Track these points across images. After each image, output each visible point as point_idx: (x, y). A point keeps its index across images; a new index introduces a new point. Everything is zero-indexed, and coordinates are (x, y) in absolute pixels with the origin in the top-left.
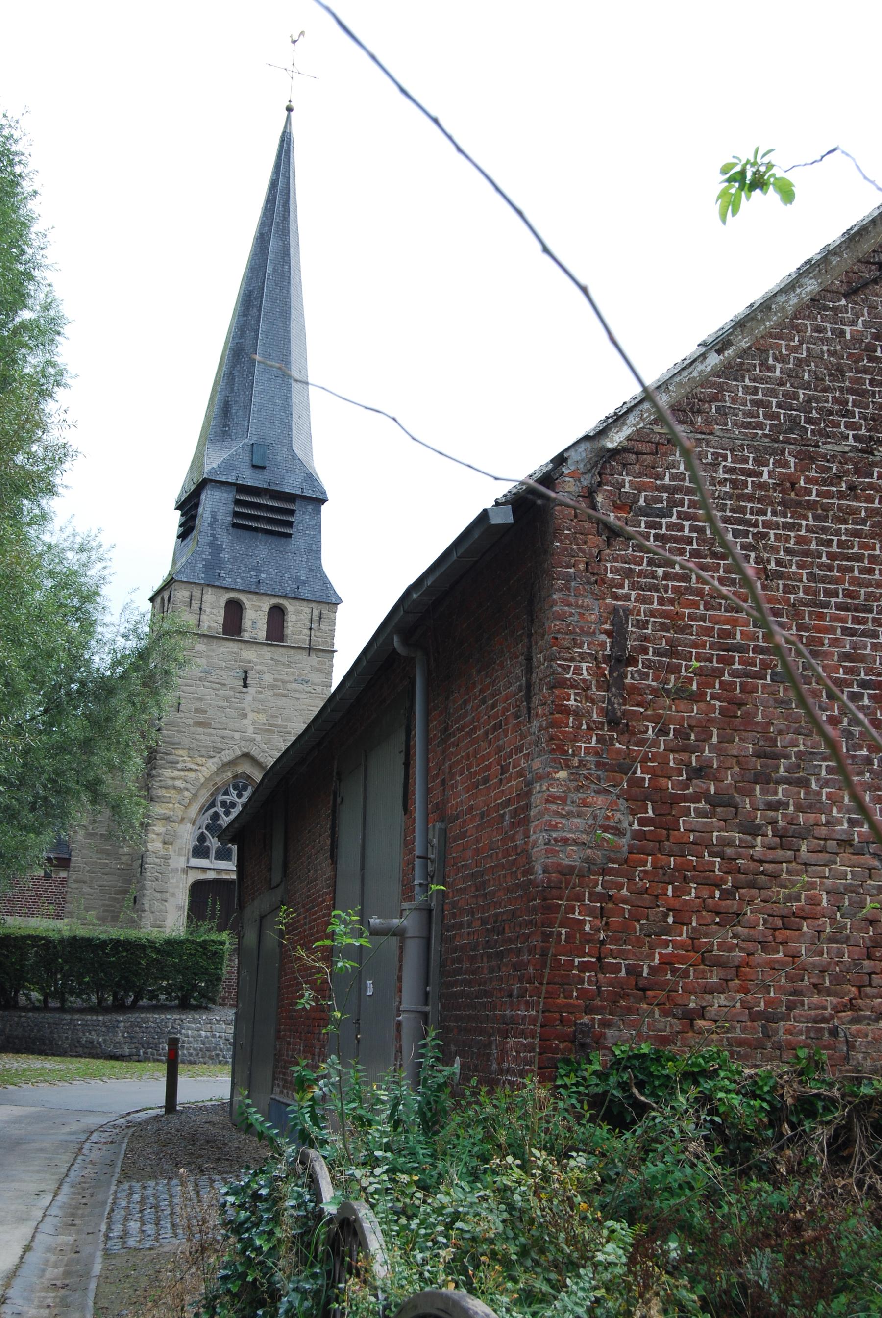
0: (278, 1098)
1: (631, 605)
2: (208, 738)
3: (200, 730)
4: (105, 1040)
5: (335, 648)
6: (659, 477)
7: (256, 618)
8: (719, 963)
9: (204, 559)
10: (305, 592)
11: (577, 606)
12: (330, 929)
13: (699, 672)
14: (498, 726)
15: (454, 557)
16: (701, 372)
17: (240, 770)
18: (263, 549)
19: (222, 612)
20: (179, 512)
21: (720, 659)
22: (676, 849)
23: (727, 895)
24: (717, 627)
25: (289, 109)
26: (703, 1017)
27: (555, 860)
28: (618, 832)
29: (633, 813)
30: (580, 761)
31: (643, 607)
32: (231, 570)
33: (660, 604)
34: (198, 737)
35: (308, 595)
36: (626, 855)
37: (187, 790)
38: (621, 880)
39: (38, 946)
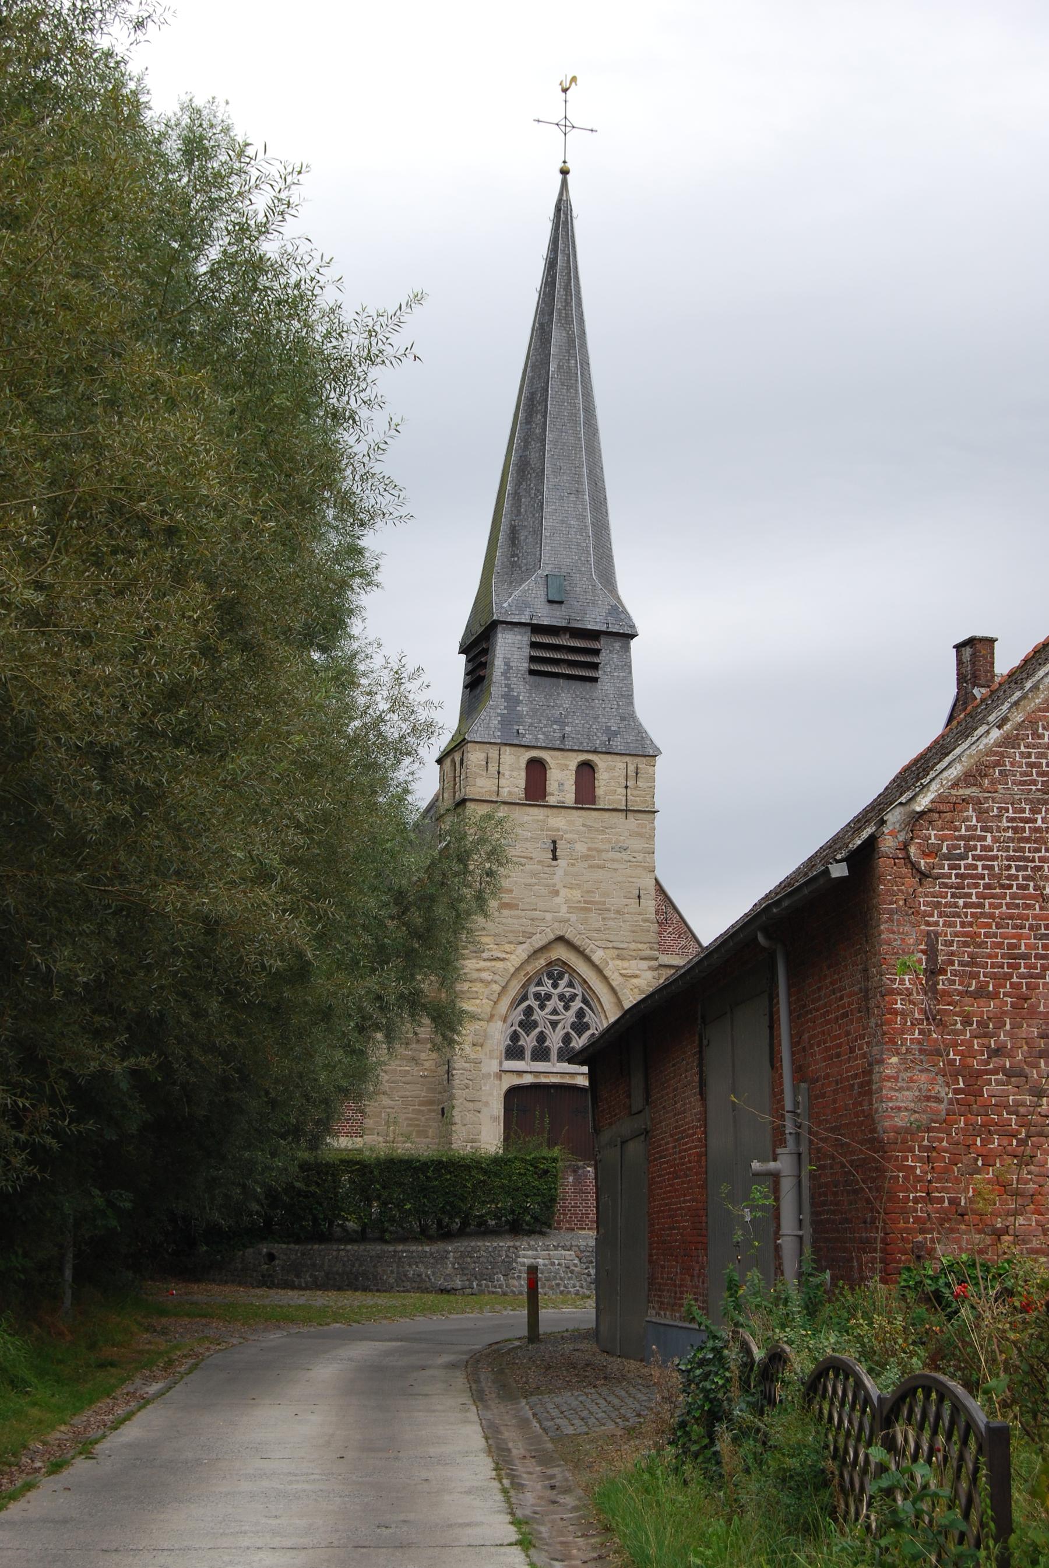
0: (654, 1320)
1: (940, 929)
2: (515, 921)
4: (434, 1273)
5: (657, 808)
6: (956, 829)
7: (561, 778)
8: (1017, 1193)
9: (499, 715)
10: (617, 744)
11: (899, 933)
12: (752, 1196)
13: (994, 976)
14: (845, 1015)
15: (806, 891)
16: (987, 744)
19: (523, 774)
20: (463, 657)
21: (1010, 966)
22: (982, 1110)
23: (1022, 1143)
24: (1006, 941)
25: (565, 172)
26: (1007, 1233)
27: (892, 1123)
28: (938, 1100)
29: (948, 1085)
30: (907, 1049)
31: (949, 930)
33: (962, 927)
34: (504, 921)
35: (621, 748)
36: (944, 1117)
37: (496, 982)
38: (941, 1135)
39: (351, 1172)
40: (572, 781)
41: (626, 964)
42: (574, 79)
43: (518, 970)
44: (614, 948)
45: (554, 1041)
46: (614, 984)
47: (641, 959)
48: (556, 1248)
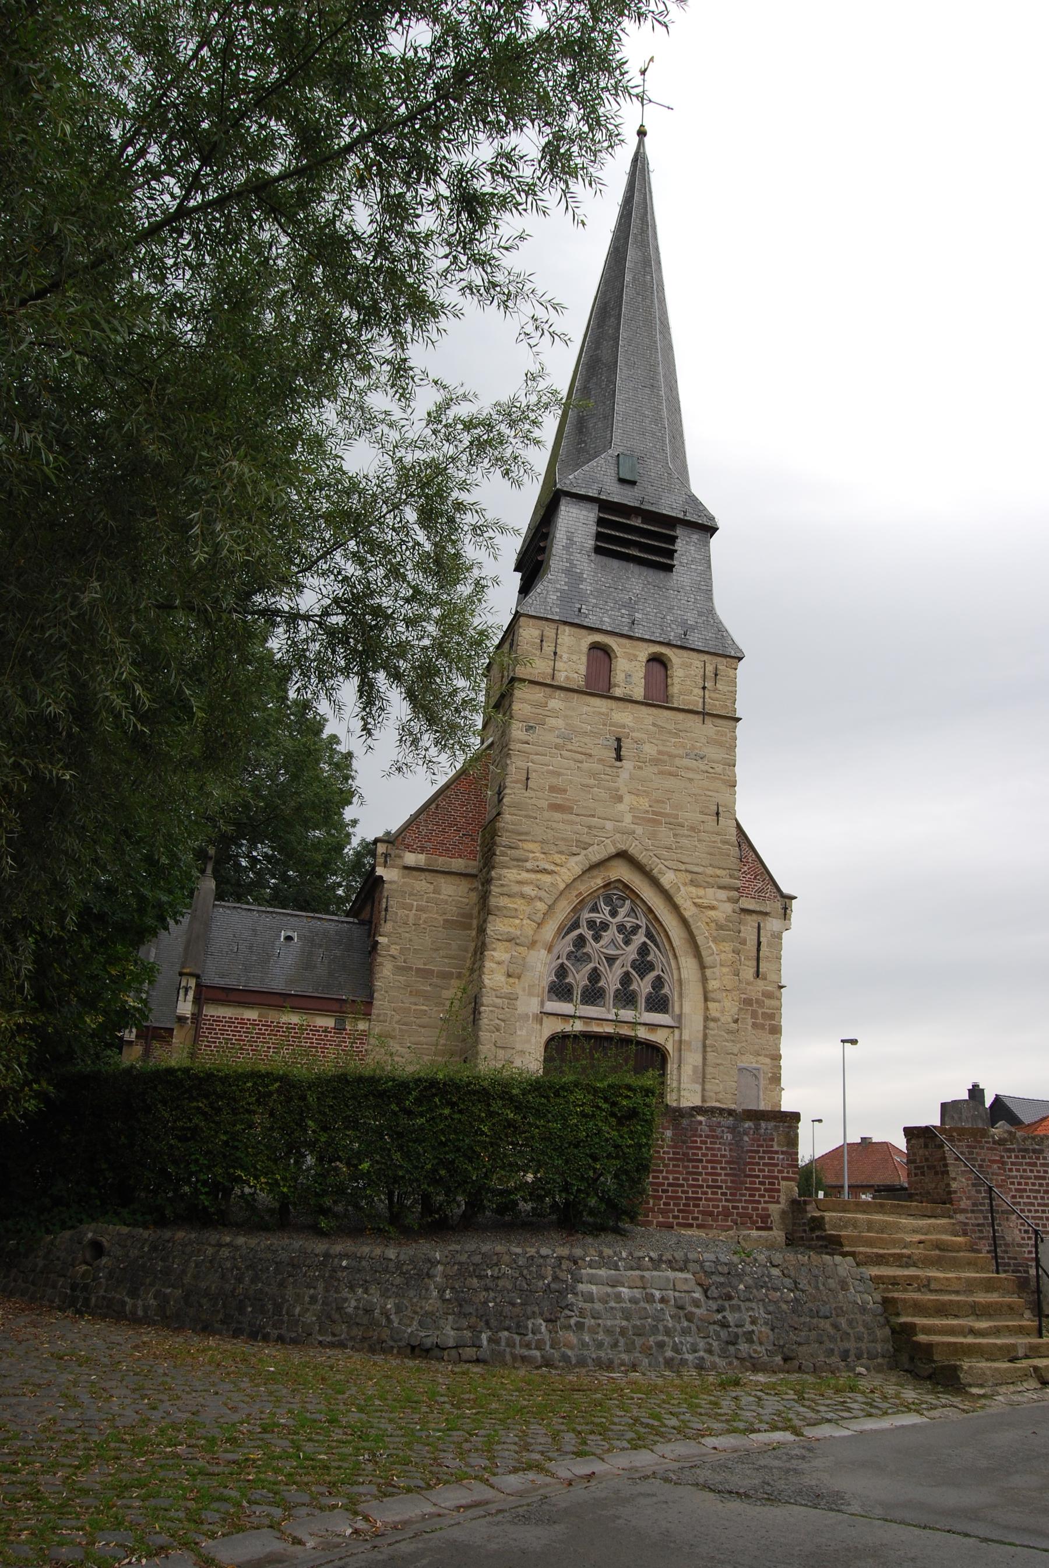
3: (557, 816)
4: (399, 1309)
7: (630, 669)
10: (695, 640)
17: (614, 875)
18: (636, 581)
19: (584, 659)
32: (595, 606)
34: (554, 825)
35: (699, 645)
37: (540, 899)
40: (642, 675)
41: (701, 892)
42: (652, 60)
43: (568, 886)
44: (687, 871)
45: (611, 981)
46: (687, 914)
47: (720, 888)
48: (656, 1264)
